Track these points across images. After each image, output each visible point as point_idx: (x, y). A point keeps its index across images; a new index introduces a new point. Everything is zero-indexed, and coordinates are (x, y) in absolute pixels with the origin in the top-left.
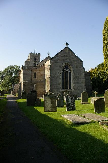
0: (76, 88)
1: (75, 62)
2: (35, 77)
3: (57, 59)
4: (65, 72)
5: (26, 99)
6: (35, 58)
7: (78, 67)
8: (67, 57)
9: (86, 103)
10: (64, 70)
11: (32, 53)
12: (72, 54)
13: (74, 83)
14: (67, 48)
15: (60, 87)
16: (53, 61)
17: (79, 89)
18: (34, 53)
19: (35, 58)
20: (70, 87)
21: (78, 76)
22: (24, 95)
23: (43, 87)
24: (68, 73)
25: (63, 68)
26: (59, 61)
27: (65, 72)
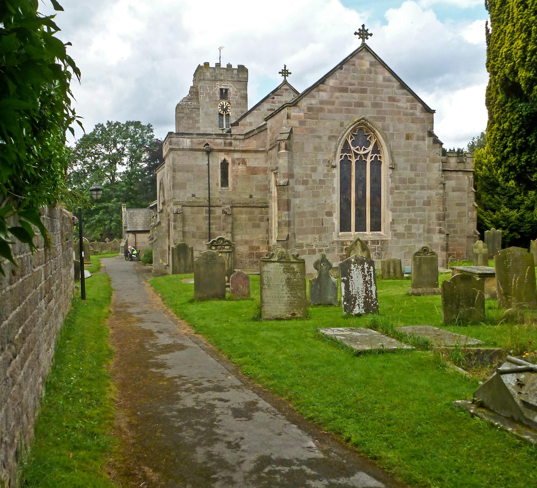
0: (401, 229)
1: (399, 113)
2: (225, 182)
3: (322, 102)
4: (354, 161)
5: (193, 275)
6: (221, 90)
7: (415, 137)
8: (363, 91)
9: (429, 289)
10: (349, 151)
11: (207, 64)
12: (385, 80)
13: (395, 206)
14: (361, 54)
15: (333, 224)
16: (302, 114)
17: (413, 231)
18: (218, 65)
19: (221, 90)
20: (376, 227)
21: (412, 175)
22: (179, 259)
23: (262, 224)
24: (353, 164)
25: (346, 142)
26: (330, 111)
27: (354, 161)
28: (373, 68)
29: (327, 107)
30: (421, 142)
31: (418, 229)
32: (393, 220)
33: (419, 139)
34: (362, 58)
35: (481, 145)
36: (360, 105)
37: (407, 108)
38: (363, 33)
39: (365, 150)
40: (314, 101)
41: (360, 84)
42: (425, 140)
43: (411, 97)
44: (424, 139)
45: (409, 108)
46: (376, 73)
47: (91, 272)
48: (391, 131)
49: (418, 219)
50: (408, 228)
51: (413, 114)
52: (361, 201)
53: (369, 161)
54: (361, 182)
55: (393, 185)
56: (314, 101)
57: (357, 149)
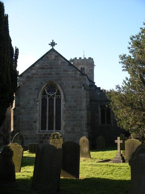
0: (69, 129)
3: (33, 74)
4: (48, 99)
12: (62, 62)
26: (36, 78)
27: (48, 99)
28: (56, 58)
29: (35, 76)
30: (79, 89)
31: (78, 129)
32: (65, 125)
33: (79, 87)
34: (51, 54)
35: (92, 79)
36: (50, 74)
37: (72, 74)
38: (53, 44)
39: (53, 93)
40: (29, 74)
41: (50, 65)
42: (82, 88)
43: (74, 69)
44: (81, 88)
45: (73, 74)
46: (58, 60)
47: (105, 106)
48: (65, 85)
49: (78, 125)
50: (73, 129)
51: (75, 77)
52: (51, 116)
53: (55, 99)
54: (51, 107)
55: (65, 109)
56: (29, 74)
57: (50, 94)
